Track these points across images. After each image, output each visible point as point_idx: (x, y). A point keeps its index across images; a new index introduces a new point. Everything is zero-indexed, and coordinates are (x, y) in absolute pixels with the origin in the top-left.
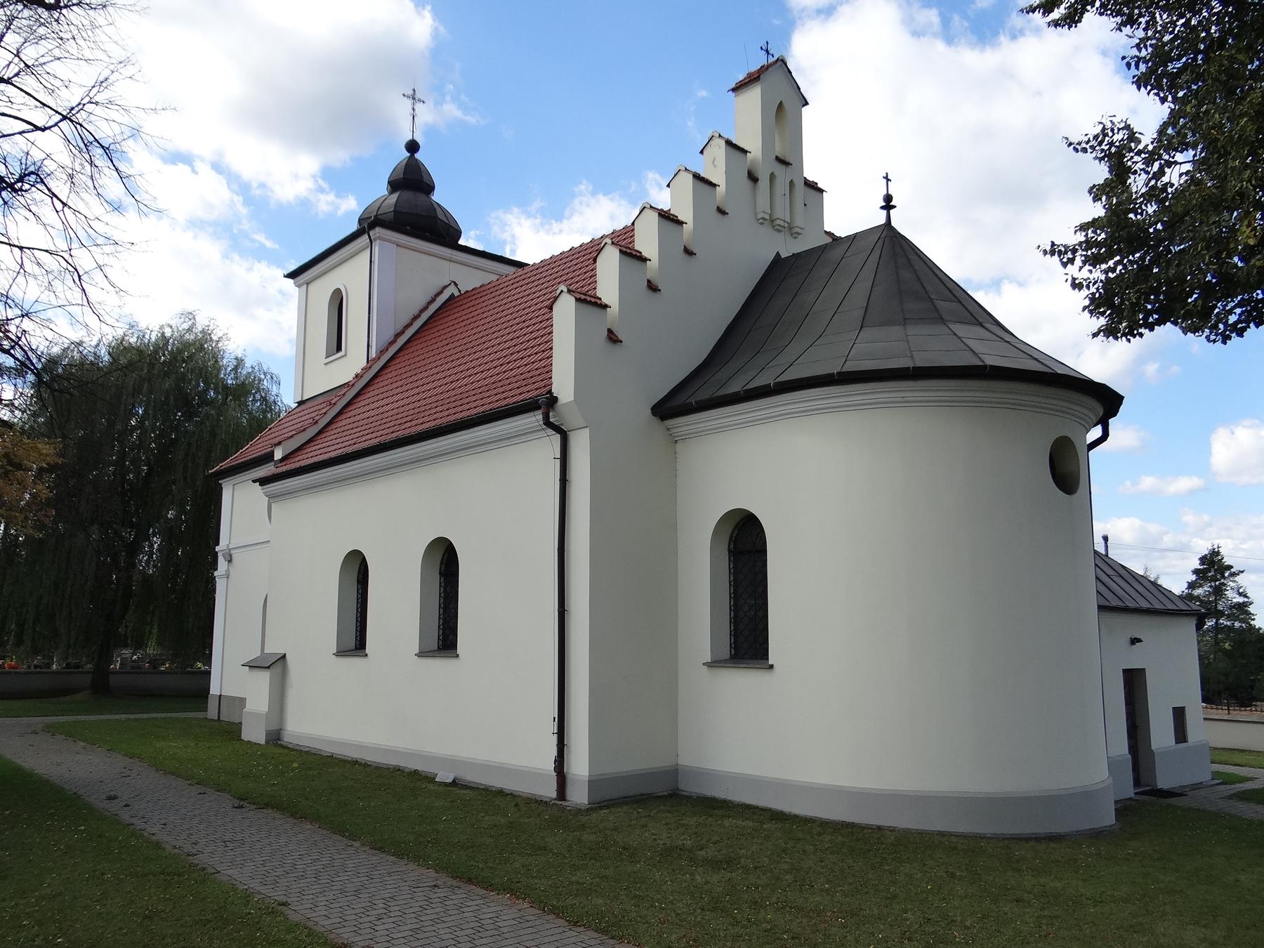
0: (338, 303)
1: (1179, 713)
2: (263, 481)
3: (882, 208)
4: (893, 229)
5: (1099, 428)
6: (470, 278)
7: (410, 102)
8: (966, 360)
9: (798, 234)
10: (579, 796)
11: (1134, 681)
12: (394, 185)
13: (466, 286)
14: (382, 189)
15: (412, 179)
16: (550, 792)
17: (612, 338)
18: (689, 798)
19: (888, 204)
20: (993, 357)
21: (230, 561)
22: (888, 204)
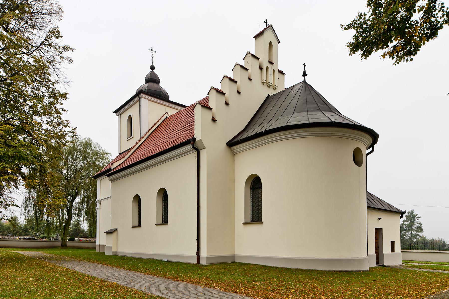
0: (130, 118)
1: (393, 244)
2: (108, 176)
3: (303, 76)
4: (306, 82)
5: (371, 148)
6: (172, 112)
7: (151, 52)
8: (327, 120)
9: (276, 88)
10: (203, 262)
11: (378, 232)
12: (147, 81)
13: (170, 114)
14: (143, 82)
15: (153, 79)
16: (195, 262)
17: (214, 120)
18: (237, 263)
19: (305, 75)
20: (334, 119)
21: (100, 204)
22: (305, 75)
